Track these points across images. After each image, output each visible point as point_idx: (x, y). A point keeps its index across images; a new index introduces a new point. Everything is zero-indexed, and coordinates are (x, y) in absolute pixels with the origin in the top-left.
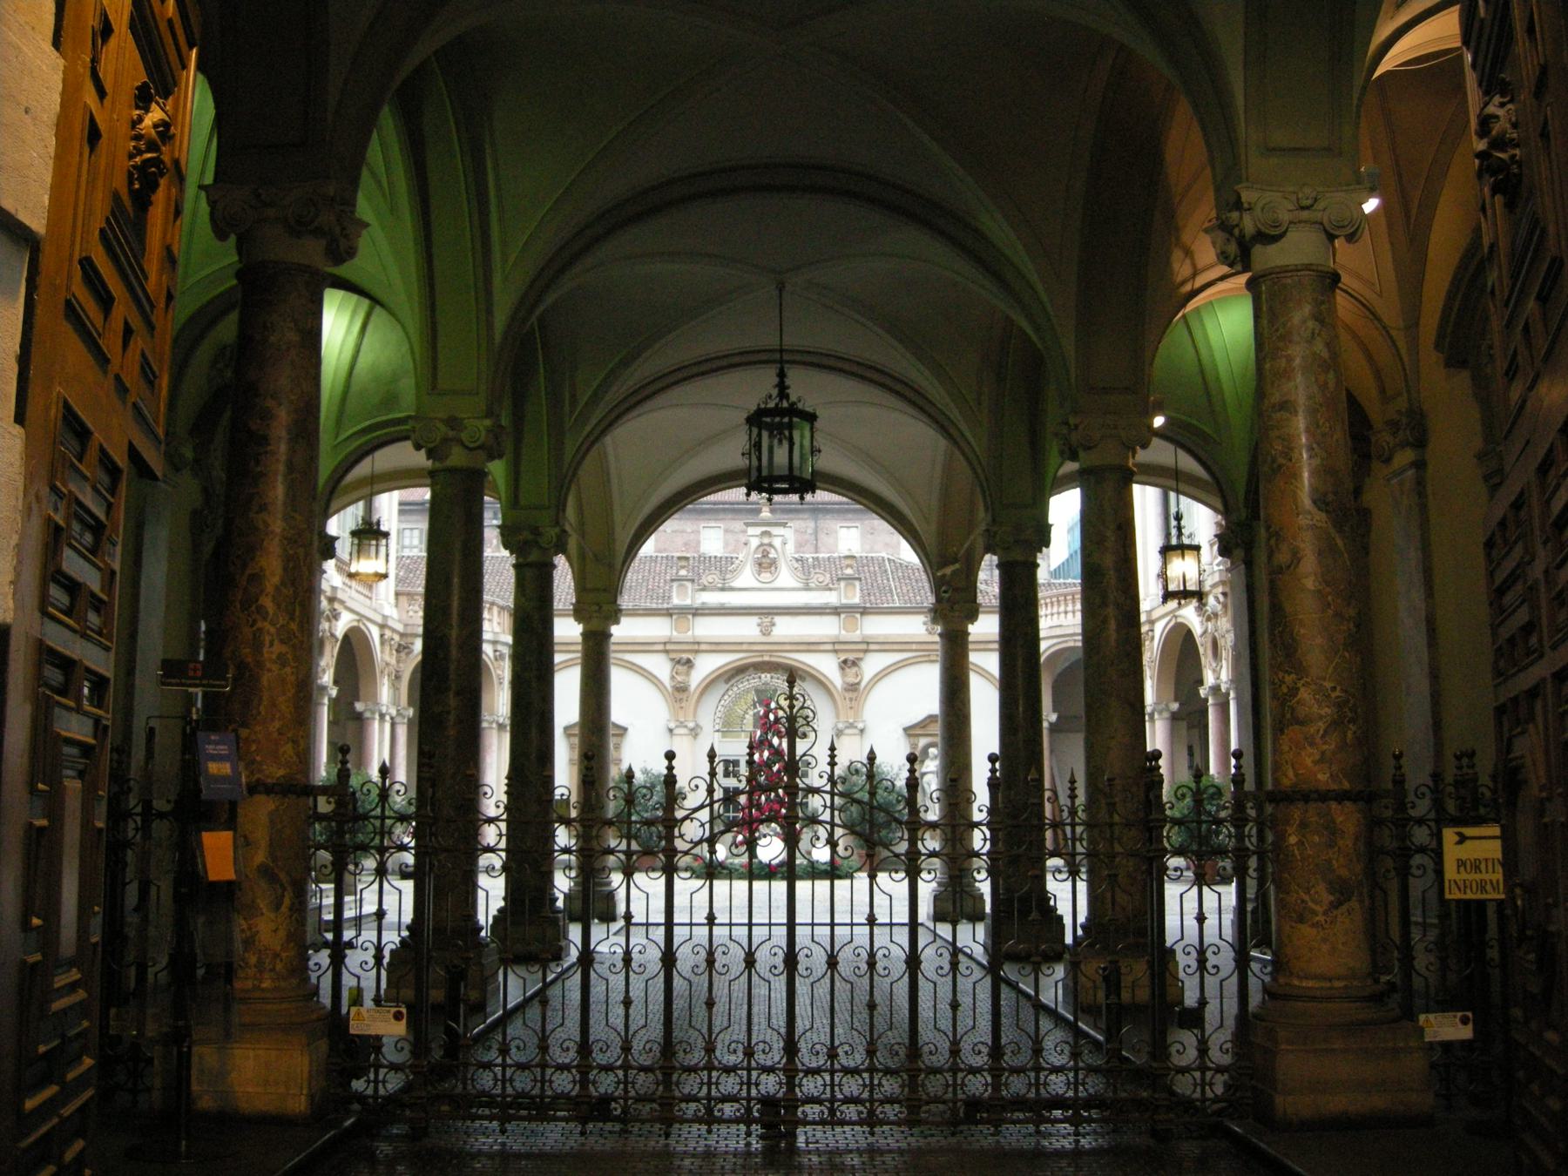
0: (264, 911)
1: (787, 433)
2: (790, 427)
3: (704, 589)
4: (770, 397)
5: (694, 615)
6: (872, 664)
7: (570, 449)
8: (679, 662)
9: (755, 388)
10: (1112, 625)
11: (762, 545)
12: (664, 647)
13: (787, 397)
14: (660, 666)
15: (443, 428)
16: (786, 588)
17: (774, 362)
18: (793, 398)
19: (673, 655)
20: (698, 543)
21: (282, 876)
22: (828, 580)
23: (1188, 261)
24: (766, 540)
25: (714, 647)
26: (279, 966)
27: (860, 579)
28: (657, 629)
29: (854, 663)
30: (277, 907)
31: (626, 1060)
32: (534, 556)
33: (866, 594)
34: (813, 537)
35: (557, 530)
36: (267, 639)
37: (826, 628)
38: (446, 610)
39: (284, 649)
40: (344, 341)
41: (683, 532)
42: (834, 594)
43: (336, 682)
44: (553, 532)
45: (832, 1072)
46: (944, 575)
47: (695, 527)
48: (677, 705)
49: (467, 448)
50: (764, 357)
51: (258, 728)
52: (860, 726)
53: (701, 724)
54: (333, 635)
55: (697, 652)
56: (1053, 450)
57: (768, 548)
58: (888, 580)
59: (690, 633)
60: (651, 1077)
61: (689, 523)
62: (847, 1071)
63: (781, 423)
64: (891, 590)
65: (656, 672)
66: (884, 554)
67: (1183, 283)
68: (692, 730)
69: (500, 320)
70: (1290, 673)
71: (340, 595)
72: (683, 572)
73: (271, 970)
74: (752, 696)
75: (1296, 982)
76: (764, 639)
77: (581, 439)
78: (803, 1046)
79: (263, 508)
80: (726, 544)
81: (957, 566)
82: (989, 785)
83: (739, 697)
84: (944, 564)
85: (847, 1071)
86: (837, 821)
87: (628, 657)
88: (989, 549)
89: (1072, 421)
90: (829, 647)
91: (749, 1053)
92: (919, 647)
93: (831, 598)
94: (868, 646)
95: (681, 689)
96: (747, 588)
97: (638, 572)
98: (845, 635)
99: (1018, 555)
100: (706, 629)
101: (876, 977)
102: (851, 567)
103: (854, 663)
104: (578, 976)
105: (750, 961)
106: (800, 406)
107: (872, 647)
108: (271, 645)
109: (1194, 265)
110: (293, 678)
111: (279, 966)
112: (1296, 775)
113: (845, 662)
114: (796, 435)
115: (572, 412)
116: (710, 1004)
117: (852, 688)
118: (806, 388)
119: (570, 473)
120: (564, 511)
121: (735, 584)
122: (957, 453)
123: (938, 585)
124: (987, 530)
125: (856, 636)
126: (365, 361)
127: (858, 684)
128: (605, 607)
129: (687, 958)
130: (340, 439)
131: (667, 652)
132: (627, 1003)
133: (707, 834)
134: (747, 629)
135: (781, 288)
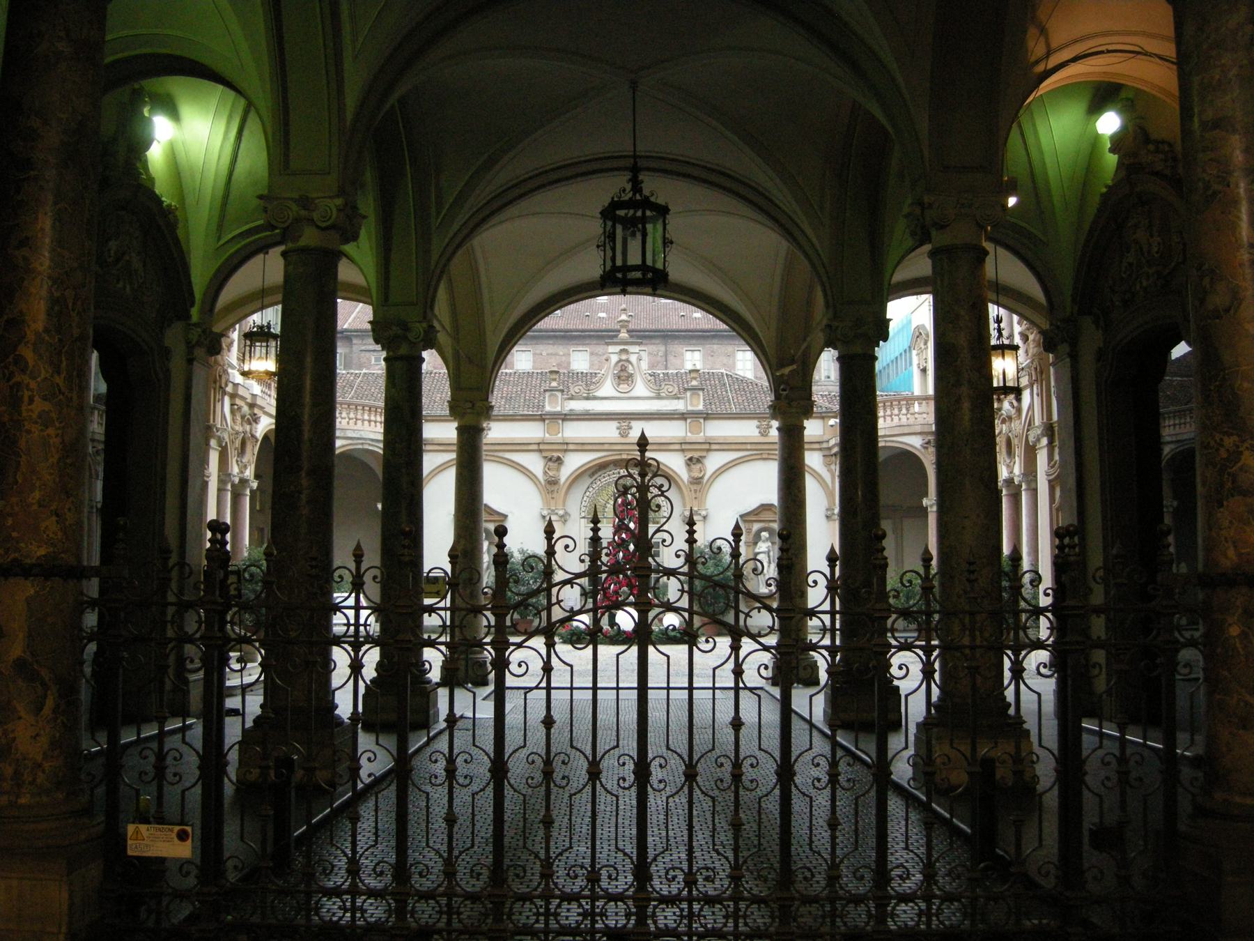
0: (23, 714)
1: (640, 226)
2: (644, 220)
3: (572, 398)
4: (624, 190)
5: (563, 420)
6: (714, 461)
7: (437, 246)
8: (550, 460)
9: (612, 186)
10: (966, 405)
11: (620, 360)
12: (539, 447)
13: (640, 191)
14: (535, 463)
15: (295, 207)
16: (640, 397)
17: (625, 169)
18: (646, 192)
19: (545, 454)
20: (569, 363)
21: (45, 674)
22: (676, 390)
23: (1042, 39)
24: (624, 357)
25: (579, 447)
26: (41, 778)
27: (703, 389)
28: (531, 431)
29: (699, 461)
30: (39, 708)
31: (450, 887)
32: (403, 350)
33: (708, 403)
34: (664, 359)
35: (425, 325)
36: (27, 394)
37: (674, 431)
38: (299, 390)
39: (47, 406)
40: (222, 146)
41: (556, 354)
42: (681, 401)
43: (257, 476)
44: (420, 328)
45: (690, 900)
46: (782, 375)
47: (566, 350)
48: (549, 496)
49: (318, 227)
50: (615, 164)
51: (14, 500)
52: (704, 513)
53: (569, 511)
54: (253, 436)
55: (566, 451)
56: (899, 231)
57: (626, 364)
58: (727, 392)
59: (560, 435)
60: (478, 907)
61: (561, 347)
62: (710, 901)
63: (634, 216)
64: (729, 400)
65: (531, 468)
66: (723, 371)
67: (1037, 62)
68: (562, 517)
69: (351, 101)
70: (1229, 435)
71: (259, 402)
72: (554, 384)
73: (32, 783)
74: (612, 489)
75: (1238, 799)
76: (623, 441)
77: (447, 240)
78: (657, 869)
79: (25, 242)
80: (592, 365)
81: (794, 367)
82: (450, 555)
83: (603, 488)
84: (782, 365)
85: (710, 901)
86: (695, 608)
87: (508, 455)
88: (830, 343)
89: (926, 200)
90: (677, 447)
91: (593, 878)
92: (754, 447)
93: (679, 405)
94: (710, 446)
95: (552, 482)
96: (608, 398)
97: (517, 386)
98: (691, 437)
99: (858, 349)
100: (574, 431)
101: (741, 792)
102: (695, 378)
103: (699, 461)
104: (447, 737)
105: (594, 773)
106: (652, 199)
107: (714, 447)
108: (31, 400)
109: (1048, 45)
110: (58, 440)
111: (41, 778)
112: (1240, 555)
113: (691, 459)
114: (649, 227)
115: (438, 213)
116: (548, 823)
117: (697, 481)
118: (657, 188)
119: (438, 271)
120: (432, 308)
121: (599, 394)
122: (799, 253)
123: (778, 384)
124: (829, 326)
125: (700, 437)
126: (242, 166)
127: (702, 478)
128: (479, 404)
129: (517, 768)
130: (222, 242)
131: (540, 451)
132: (451, 820)
133: (544, 624)
134: (607, 432)
135: (634, 85)
